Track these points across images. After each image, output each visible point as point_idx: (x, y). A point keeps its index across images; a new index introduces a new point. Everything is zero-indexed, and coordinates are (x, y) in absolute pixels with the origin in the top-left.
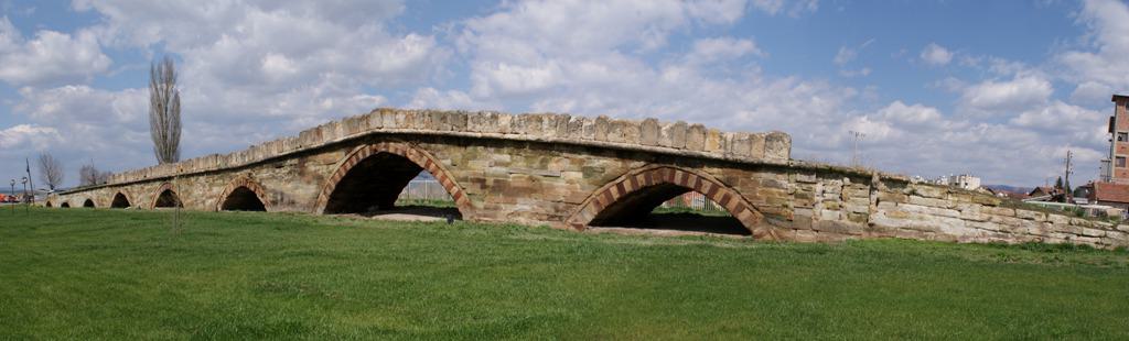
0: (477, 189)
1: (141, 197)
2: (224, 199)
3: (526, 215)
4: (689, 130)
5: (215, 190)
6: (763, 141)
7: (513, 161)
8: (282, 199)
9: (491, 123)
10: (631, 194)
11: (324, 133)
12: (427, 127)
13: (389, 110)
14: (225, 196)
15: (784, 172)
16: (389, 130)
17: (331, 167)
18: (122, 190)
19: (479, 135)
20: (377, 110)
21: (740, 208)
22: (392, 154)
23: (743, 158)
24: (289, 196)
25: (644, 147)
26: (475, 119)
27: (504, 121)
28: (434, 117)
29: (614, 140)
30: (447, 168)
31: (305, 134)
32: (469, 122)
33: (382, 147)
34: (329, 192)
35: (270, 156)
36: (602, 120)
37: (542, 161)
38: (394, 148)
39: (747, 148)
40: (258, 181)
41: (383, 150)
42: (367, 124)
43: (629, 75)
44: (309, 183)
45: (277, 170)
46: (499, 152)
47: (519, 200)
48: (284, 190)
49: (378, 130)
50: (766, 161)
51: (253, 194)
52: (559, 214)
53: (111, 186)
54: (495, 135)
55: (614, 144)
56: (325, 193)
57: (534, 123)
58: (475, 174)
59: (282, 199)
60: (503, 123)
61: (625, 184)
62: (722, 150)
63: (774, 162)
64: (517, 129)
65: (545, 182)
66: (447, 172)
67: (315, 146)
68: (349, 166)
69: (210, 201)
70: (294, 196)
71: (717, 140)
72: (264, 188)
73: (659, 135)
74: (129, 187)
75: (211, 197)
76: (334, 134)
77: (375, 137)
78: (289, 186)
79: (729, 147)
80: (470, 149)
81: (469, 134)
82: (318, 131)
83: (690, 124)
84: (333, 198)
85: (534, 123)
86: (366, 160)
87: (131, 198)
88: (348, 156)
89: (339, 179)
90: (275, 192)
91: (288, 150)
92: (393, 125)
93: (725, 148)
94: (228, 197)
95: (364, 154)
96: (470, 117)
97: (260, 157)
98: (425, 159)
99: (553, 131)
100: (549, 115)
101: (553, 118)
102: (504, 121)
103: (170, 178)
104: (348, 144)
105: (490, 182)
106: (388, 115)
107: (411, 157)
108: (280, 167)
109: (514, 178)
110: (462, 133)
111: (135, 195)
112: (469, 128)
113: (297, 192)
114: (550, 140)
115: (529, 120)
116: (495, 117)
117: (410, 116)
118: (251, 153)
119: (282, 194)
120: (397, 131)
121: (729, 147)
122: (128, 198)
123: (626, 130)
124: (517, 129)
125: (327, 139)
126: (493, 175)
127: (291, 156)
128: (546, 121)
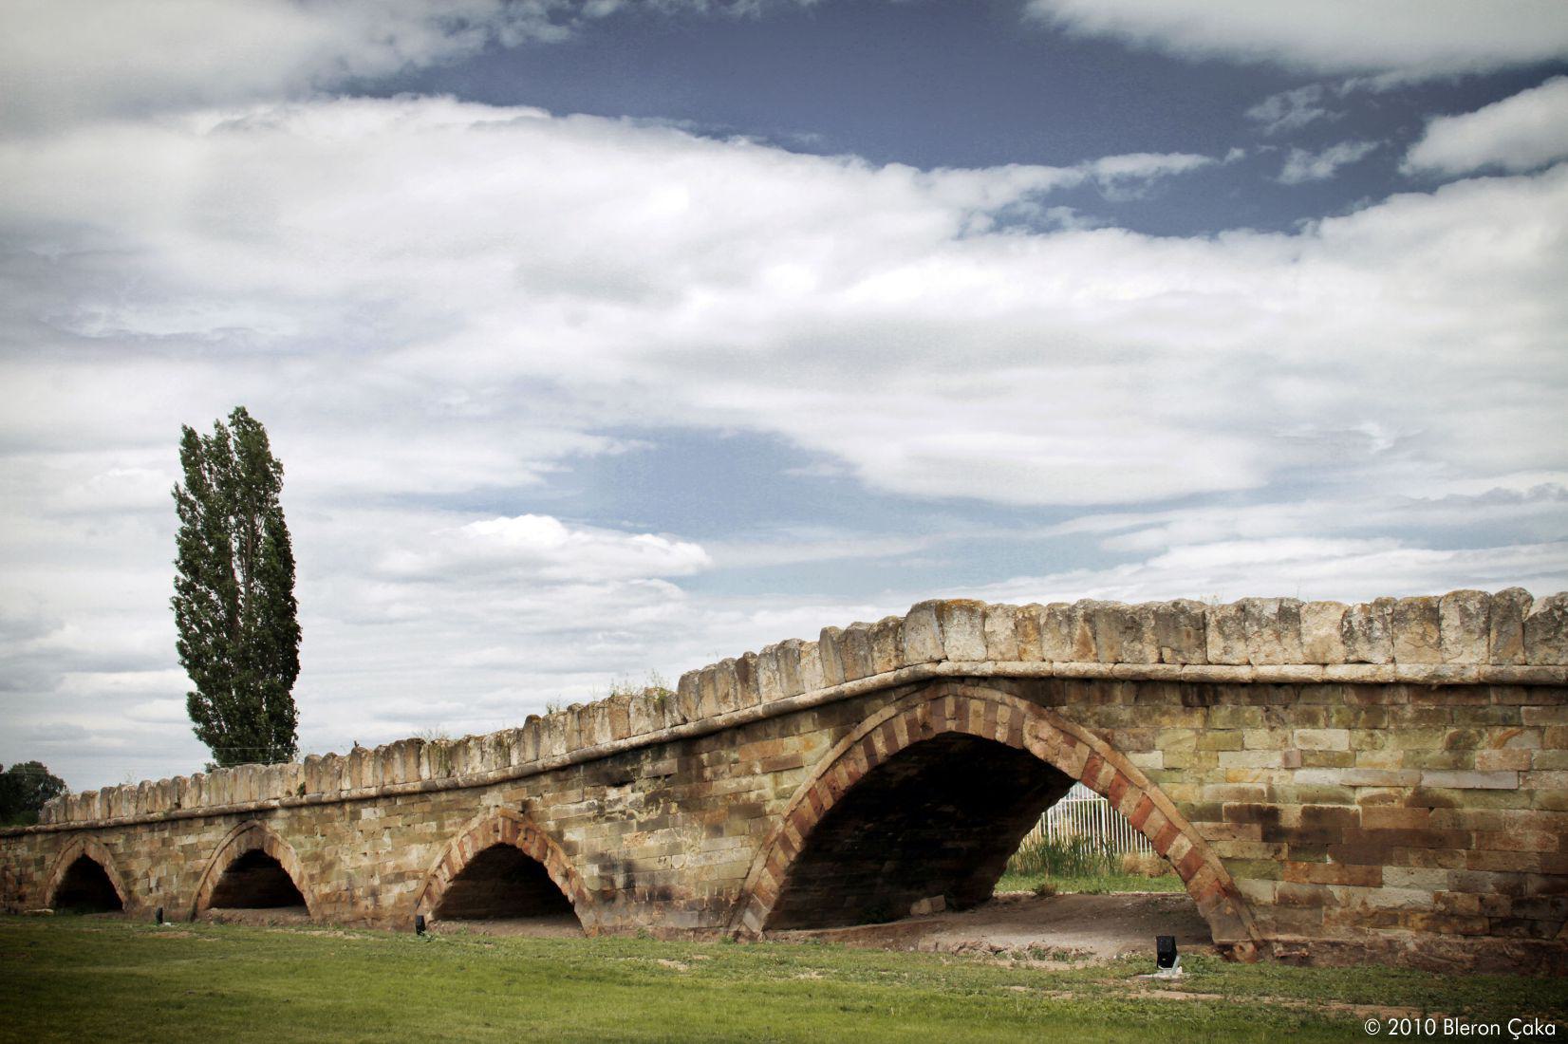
0: (1249, 844)
1: (161, 871)
2: (444, 882)
3: (1416, 919)
5: (415, 855)
8: (630, 885)
11: (763, 676)
12: (1082, 656)
14: (445, 875)
16: (966, 668)
17: (787, 781)
19: (1244, 673)
22: (977, 739)
24: (652, 877)
26: (1230, 627)
27: (1321, 630)
28: (1101, 625)
30: (1154, 777)
31: (695, 683)
32: (1213, 635)
34: (783, 859)
35: (589, 749)
37: (1453, 744)
40: (551, 825)
41: (951, 726)
42: (900, 651)
43: (1428, 746)
44: (716, 830)
45: (613, 793)
47: (1390, 872)
48: (636, 857)
49: (928, 668)
51: (535, 871)
52: (1528, 912)
54: (1294, 671)
56: (769, 862)
58: (1242, 794)
59: (630, 885)
64: (1363, 650)
66: (1152, 792)
67: (720, 721)
68: (843, 778)
69: (397, 889)
70: (667, 877)
72: (570, 849)
74: (119, 840)
75: (400, 877)
76: (792, 677)
77: (928, 685)
81: (1214, 671)
82: (744, 670)
84: (798, 877)
86: (898, 757)
87: (126, 875)
88: (841, 747)
90: (607, 863)
92: (979, 652)
94: (456, 878)
95: (890, 738)
96: (1212, 620)
98: (1084, 752)
103: (265, 812)
104: (837, 711)
107: (1037, 749)
108: (619, 784)
109: (1365, 801)
110: (1193, 670)
111: (138, 867)
112: (1214, 652)
113: (677, 862)
114: (1472, 674)
119: (629, 867)
122: (115, 877)
124: (1363, 650)
125: (771, 693)
127: (657, 747)
128: (1451, 617)
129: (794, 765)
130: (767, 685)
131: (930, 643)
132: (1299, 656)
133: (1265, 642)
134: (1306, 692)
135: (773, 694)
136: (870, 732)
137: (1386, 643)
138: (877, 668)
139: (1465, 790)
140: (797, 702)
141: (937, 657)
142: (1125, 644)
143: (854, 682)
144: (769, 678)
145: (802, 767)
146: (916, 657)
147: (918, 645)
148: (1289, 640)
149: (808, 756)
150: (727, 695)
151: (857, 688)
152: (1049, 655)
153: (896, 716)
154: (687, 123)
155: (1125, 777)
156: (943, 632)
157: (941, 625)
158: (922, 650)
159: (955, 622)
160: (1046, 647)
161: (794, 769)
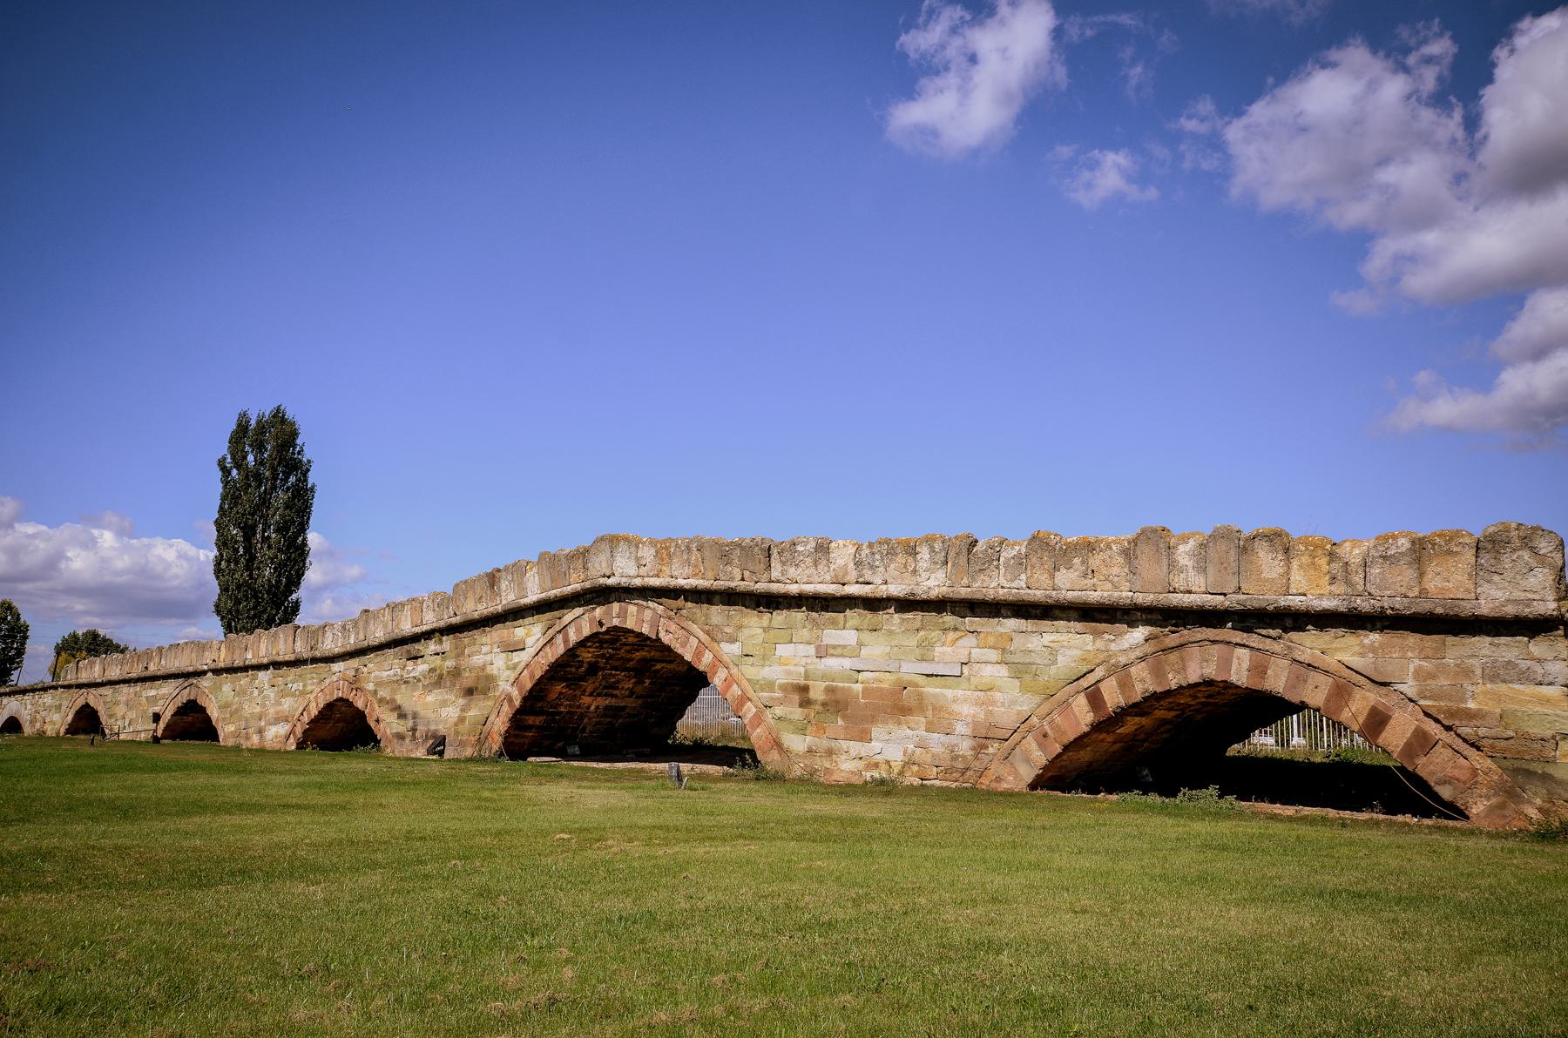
4: (1245, 547)
6: (1469, 555)
9: (816, 563)
10: (1123, 713)
11: (504, 585)
13: (626, 539)
18: (93, 698)
20: (602, 539)
21: (1421, 742)
23: (1398, 603)
25: (1140, 599)
29: (1069, 585)
31: (465, 587)
32: (775, 563)
36: (1039, 542)
38: (637, 617)
39: (1410, 574)
41: (616, 622)
42: (585, 568)
46: (834, 624)
49: (603, 581)
50: (1485, 608)
53: (69, 687)
55: (1070, 596)
57: (901, 559)
60: (840, 562)
61: (1103, 686)
62: (1339, 588)
63: (1510, 610)
64: (868, 576)
65: (931, 689)
71: (1323, 562)
73: (1172, 565)
78: (430, 698)
79: (1358, 579)
80: (780, 617)
83: (1247, 531)
85: (901, 559)
89: (529, 686)
91: (430, 620)
93: (1348, 583)
97: (379, 634)
99: (941, 575)
100: (929, 540)
101: (938, 546)
102: (842, 555)
103: (200, 674)
105: (817, 693)
106: (623, 546)
112: (775, 574)
115: (892, 553)
116: (823, 549)
117: (664, 551)
118: (361, 624)
121: (1358, 579)
123: (1095, 561)
125: (508, 597)
126: (824, 677)
128: (924, 553)
129: (518, 648)
132: (828, 578)
139: (927, 675)
145: (524, 649)
147: (597, 565)
159: (620, 549)
161: (907, 604)
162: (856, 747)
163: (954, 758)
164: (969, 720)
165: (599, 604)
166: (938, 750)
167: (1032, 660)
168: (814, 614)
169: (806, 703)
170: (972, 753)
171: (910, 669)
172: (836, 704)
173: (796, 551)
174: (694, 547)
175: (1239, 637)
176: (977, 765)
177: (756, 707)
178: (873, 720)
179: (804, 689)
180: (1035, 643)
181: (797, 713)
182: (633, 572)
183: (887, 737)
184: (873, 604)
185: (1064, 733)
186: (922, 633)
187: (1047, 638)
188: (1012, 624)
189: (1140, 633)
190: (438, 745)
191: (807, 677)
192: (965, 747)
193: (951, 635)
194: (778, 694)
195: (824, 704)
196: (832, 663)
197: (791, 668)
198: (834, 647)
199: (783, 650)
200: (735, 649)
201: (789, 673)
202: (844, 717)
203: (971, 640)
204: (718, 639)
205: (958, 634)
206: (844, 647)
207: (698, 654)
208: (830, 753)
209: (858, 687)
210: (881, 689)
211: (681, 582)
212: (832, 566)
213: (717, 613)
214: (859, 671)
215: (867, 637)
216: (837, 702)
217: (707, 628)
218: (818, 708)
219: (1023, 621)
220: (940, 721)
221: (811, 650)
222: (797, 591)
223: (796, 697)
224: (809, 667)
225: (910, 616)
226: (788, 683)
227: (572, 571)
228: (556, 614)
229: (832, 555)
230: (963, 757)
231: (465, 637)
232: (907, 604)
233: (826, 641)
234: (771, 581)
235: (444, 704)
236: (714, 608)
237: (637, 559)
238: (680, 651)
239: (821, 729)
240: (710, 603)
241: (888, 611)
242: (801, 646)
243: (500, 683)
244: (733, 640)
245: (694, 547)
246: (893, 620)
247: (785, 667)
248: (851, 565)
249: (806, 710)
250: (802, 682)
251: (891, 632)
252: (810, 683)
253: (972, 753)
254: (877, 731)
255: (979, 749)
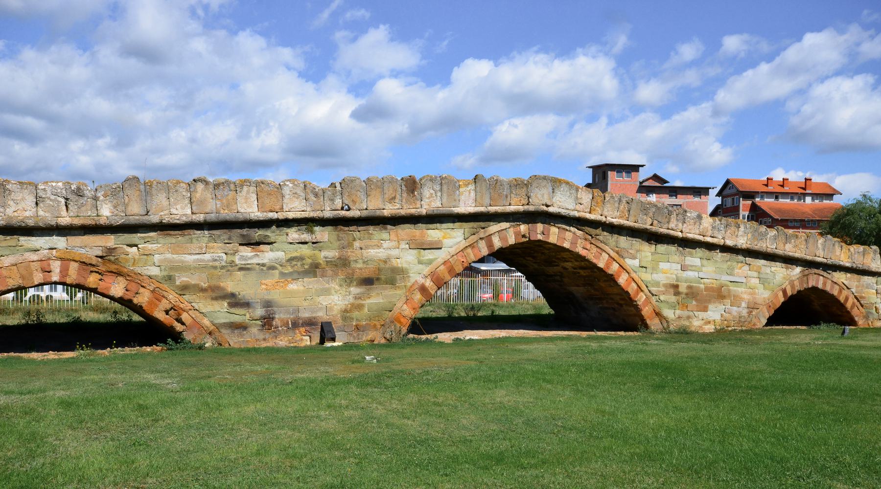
7: (702, 266)
11: (427, 192)
12: (621, 217)
13: (567, 183)
15: (674, 244)
17: (428, 255)
19: (680, 235)
33: (539, 232)
38: (554, 235)
41: (540, 237)
46: (691, 255)
49: (545, 208)
64: (716, 234)
65: (733, 288)
80: (662, 248)
82: (412, 185)
105: (683, 288)
112: (672, 225)
120: (577, 214)
126: (686, 281)
129: (436, 247)
130: (429, 198)
131: (546, 196)
132: (698, 232)
133: (690, 225)
134: (40, 260)
135: (433, 204)
136: (491, 234)
137: (723, 232)
138: (513, 202)
139: (731, 282)
140: (456, 212)
141: (549, 204)
142: (641, 215)
143: (499, 207)
144: (432, 194)
145: (441, 248)
146: (538, 202)
147: (539, 196)
148: (697, 226)
149: (447, 242)
150: (394, 198)
151: (499, 211)
152: (605, 213)
153: (509, 228)
154: (535, 48)
155: (640, 288)
156: (553, 192)
157: (553, 189)
158: (541, 199)
159: (562, 189)
160: (606, 210)
161: (725, 249)
162: (701, 315)
163: (740, 317)
164: (747, 301)
165: (524, 223)
166: (735, 314)
167: (767, 277)
168: (681, 249)
169: (677, 293)
170: (747, 314)
171: (725, 278)
172: (692, 293)
173: (686, 216)
174: (624, 200)
175: (822, 273)
176: (749, 319)
177: (646, 295)
178: (709, 302)
179: (676, 287)
180: (768, 270)
181: (673, 299)
182: (571, 207)
183: (715, 309)
184: (710, 247)
185: (776, 305)
186: (729, 263)
187: (773, 269)
188: (763, 262)
189: (798, 269)
190: (326, 333)
191: (677, 280)
192: (745, 312)
193: (740, 265)
194: (662, 289)
195: (687, 294)
196: (691, 274)
197: (668, 275)
198: (692, 266)
199: (663, 266)
200: (636, 263)
201: (668, 278)
202: (696, 300)
203: (746, 267)
204: (624, 256)
205: (743, 264)
206: (696, 266)
207: (608, 265)
208: (689, 317)
209: (702, 286)
210: (712, 287)
211: (610, 220)
212: (701, 227)
213: (624, 241)
214: (702, 278)
215: (705, 262)
216: (693, 293)
217: (617, 249)
218: (683, 296)
219: (766, 261)
220: (736, 300)
221: (679, 266)
222: (523, 210)
223: (672, 291)
224: (679, 275)
225: (725, 254)
226: (668, 283)
227: (513, 195)
228: (482, 224)
229: (703, 221)
230: (744, 316)
231: (356, 232)
232: (725, 249)
233: (687, 263)
234: (668, 229)
235: (326, 292)
236: (622, 238)
237: (577, 198)
238: (595, 261)
239: (685, 307)
240: (620, 234)
241: (717, 251)
242: (674, 264)
243: (411, 275)
244: (634, 258)
245: (624, 200)
246: (718, 255)
247: (666, 275)
248: (710, 228)
249: (677, 297)
250: (675, 283)
251: (716, 261)
252: (679, 283)
253: (747, 314)
254: (711, 307)
255: (750, 313)
